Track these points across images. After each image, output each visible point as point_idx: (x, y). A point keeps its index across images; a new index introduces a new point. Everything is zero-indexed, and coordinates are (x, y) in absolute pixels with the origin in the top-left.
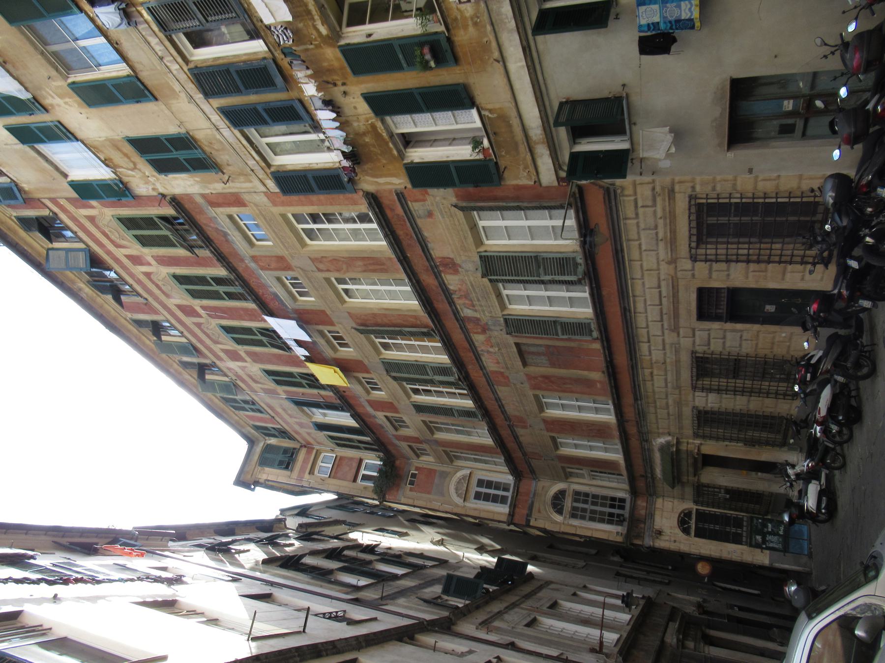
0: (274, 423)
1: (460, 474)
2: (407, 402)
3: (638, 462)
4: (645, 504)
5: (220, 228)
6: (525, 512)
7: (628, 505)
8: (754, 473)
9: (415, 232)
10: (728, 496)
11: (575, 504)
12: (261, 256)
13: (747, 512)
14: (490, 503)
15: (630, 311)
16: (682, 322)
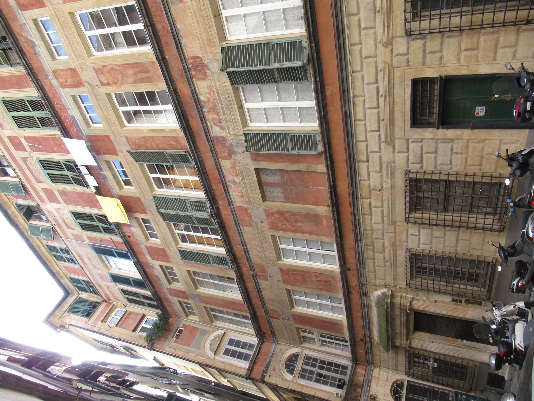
0: (83, 276)
1: (217, 333)
2: (175, 247)
3: (358, 322)
4: (363, 372)
5: (30, 38)
6: (263, 368)
7: (349, 372)
8: (460, 340)
9: (170, 23)
10: (436, 365)
11: (305, 367)
12: (59, 70)
13: (453, 387)
14: (235, 359)
15: (350, 117)
16: (398, 133)
